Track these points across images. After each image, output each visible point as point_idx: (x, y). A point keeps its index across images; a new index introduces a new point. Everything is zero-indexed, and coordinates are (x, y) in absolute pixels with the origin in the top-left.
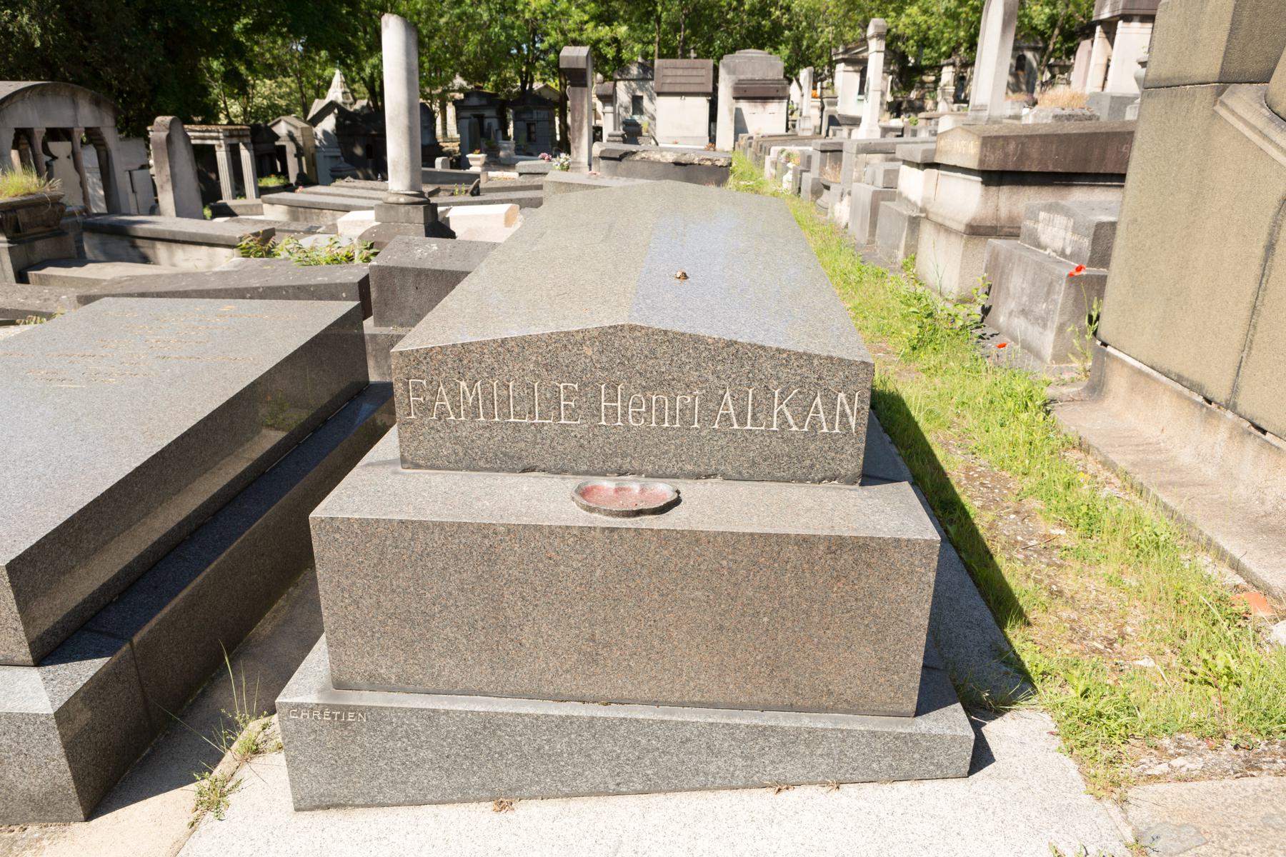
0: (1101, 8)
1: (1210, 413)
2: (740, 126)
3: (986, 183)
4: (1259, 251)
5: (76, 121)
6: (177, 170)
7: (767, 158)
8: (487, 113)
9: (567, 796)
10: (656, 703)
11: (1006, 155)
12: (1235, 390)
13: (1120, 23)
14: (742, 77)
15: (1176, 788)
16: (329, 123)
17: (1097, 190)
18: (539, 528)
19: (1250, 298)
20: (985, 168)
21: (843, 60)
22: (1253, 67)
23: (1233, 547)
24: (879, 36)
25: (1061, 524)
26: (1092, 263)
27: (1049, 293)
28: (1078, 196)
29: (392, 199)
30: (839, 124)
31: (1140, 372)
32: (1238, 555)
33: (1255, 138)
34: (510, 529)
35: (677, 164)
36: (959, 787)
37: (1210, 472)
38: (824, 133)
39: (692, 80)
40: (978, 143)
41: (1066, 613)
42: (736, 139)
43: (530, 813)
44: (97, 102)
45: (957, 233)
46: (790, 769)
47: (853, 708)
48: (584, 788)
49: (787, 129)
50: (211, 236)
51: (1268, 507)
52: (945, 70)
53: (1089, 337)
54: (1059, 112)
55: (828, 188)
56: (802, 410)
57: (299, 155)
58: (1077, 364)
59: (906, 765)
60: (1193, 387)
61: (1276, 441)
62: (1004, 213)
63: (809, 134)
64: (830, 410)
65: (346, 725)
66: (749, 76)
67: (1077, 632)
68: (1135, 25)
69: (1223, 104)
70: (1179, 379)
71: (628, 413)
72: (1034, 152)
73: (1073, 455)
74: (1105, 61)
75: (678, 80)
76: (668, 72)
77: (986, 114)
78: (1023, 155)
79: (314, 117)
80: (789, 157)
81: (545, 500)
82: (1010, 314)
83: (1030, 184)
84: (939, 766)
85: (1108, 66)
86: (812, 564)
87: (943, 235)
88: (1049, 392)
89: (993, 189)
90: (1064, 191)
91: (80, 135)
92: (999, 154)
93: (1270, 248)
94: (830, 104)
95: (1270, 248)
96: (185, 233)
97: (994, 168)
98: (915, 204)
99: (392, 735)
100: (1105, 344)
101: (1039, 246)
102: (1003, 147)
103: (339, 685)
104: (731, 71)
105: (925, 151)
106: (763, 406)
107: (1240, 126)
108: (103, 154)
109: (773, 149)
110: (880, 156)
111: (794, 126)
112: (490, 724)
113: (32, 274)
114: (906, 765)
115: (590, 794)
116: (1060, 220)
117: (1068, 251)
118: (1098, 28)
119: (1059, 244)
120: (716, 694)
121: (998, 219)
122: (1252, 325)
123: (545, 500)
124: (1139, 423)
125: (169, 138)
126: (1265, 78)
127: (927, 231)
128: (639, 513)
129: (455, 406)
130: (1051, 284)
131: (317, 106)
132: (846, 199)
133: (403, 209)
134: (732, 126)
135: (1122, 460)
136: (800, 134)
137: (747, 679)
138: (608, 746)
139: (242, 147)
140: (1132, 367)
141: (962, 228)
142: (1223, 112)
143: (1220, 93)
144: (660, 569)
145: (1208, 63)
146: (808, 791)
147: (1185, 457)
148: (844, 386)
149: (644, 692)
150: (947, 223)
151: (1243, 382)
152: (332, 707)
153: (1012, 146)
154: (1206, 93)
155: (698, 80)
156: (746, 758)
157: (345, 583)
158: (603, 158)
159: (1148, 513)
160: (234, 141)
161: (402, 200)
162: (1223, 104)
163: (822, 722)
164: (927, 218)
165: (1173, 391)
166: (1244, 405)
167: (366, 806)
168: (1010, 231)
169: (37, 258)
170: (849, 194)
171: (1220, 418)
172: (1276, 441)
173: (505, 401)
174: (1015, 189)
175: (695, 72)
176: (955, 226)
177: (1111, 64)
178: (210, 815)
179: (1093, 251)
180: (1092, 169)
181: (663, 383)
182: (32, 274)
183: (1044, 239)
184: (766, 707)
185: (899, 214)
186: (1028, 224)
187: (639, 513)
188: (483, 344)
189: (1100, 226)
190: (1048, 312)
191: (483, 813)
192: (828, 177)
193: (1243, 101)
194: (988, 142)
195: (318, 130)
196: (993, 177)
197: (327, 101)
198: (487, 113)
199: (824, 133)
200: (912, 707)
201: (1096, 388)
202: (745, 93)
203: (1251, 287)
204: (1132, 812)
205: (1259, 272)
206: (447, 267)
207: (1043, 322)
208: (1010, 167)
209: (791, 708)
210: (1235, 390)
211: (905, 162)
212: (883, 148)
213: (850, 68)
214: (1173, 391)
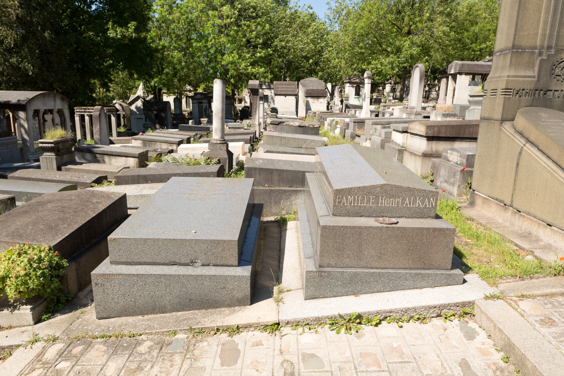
0: (451, 69)
1: (506, 208)
2: (308, 108)
4: (515, 165)
5: (55, 106)
6: (101, 127)
7: (325, 122)
8: (204, 101)
9: (372, 293)
10: (394, 268)
11: (434, 131)
12: (512, 201)
13: (458, 75)
14: (308, 88)
15: (507, 284)
16: (139, 103)
18: (372, 227)
19: (514, 177)
21: (349, 82)
22: (509, 117)
23: (516, 241)
24: (369, 78)
25: (469, 239)
26: (467, 166)
27: (454, 176)
28: (458, 145)
29: (215, 142)
30: (349, 108)
31: (485, 198)
32: (516, 242)
33: (511, 136)
34: (365, 227)
35: (299, 126)
36: (461, 286)
37: (507, 224)
39: (289, 89)
40: (425, 127)
41: (476, 257)
42: (307, 113)
44: (62, 99)
45: (419, 156)
46: (424, 283)
47: (437, 269)
48: (376, 290)
49: (328, 109)
50: (127, 153)
51: (523, 231)
52: (387, 85)
53: (468, 189)
54: (444, 112)
55: (359, 136)
56: (423, 202)
57: (124, 117)
58: (465, 197)
59: (449, 281)
60: (501, 201)
61: (523, 214)
62: (434, 149)
63: (338, 112)
64: (429, 202)
65: (322, 276)
66: (312, 88)
67: (479, 261)
68: (463, 76)
70: (497, 200)
71: (384, 202)
72: (443, 130)
73: (469, 222)
74: (453, 88)
75: (284, 89)
76: (279, 86)
78: (439, 132)
79: (131, 102)
80: (337, 123)
81: (371, 222)
82: (441, 182)
83: (442, 141)
84: (456, 281)
85: (454, 90)
86: (429, 234)
87: (413, 157)
88: (459, 205)
89: (430, 142)
90: (453, 143)
91: (55, 110)
92: (432, 131)
93: (518, 164)
94: (346, 100)
95: (518, 164)
96: (116, 152)
98: (399, 145)
99: (332, 278)
100: (474, 191)
101: (449, 161)
103: (320, 266)
104: (304, 86)
106: (415, 201)
107: (508, 133)
108: (63, 119)
109: (328, 119)
110: (380, 126)
111: (331, 108)
112: (356, 274)
113: (63, 168)
114: (449, 281)
115: (377, 292)
116: (455, 153)
117: (459, 163)
118: (450, 77)
119: (456, 161)
120: (407, 266)
121: (432, 151)
122: (515, 184)
123: (371, 222)
124: (486, 212)
125: (100, 114)
126: (513, 120)
127: (406, 156)
128: (392, 224)
129: (347, 202)
130: (455, 173)
131: (132, 97)
132: (368, 141)
133: (218, 145)
134: (305, 107)
135: (483, 222)
136: (335, 112)
137: (414, 262)
138: (382, 279)
139: (112, 116)
140: (483, 197)
141: (421, 154)
142: (503, 129)
143: (502, 123)
144: (397, 236)
145: (498, 115)
146: (427, 289)
147: (500, 221)
148: (432, 197)
149: (391, 266)
150: (414, 152)
151: (514, 199)
152: (319, 272)
153: (436, 129)
154: (497, 123)
155: (292, 90)
156: (413, 281)
157: (326, 241)
158: (272, 124)
159: (493, 234)
160: (110, 113)
161: (218, 142)
163: (430, 272)
164: (406, 150)
165: (495, 203)
166: (515, 205)
167: (323, 298)
168: (438, 155)
169: (64, 161)
170: (370, 139)
171: (509, 209)
172: (523, 214)
173: (358, 201)
174: (437, 142)
175: (290, 87)
176: (417, 153)
177: (456, 90)
178: (280, 303)
179: (467, 163)
180: (461, 136)
181: (393, 196)
182: (63, 168)
183: (450, 159)
184: (418, 269)
185: (394, 148)
186: (444, 154)
187: (392, 224)
188: (355, 188)
189: (468, 156)
190: (454, 181)
191: (353, 297)
192: (358, 132)
193: (507, 126)
194: (428, 127)
195: (133, 107)
196: (430, 138)
197: (136, 96)
198: (204, 101)
200: (450, 268)
201: (472, 203)
202: (311, 94)
203: (514, 174)
204: (499, 288)
206: (269, 167)
207: (453, 184)
208: (436, 135)
209: (424, 269)
210: (512, 201)
211: (394, 130)
214: (495, 203)
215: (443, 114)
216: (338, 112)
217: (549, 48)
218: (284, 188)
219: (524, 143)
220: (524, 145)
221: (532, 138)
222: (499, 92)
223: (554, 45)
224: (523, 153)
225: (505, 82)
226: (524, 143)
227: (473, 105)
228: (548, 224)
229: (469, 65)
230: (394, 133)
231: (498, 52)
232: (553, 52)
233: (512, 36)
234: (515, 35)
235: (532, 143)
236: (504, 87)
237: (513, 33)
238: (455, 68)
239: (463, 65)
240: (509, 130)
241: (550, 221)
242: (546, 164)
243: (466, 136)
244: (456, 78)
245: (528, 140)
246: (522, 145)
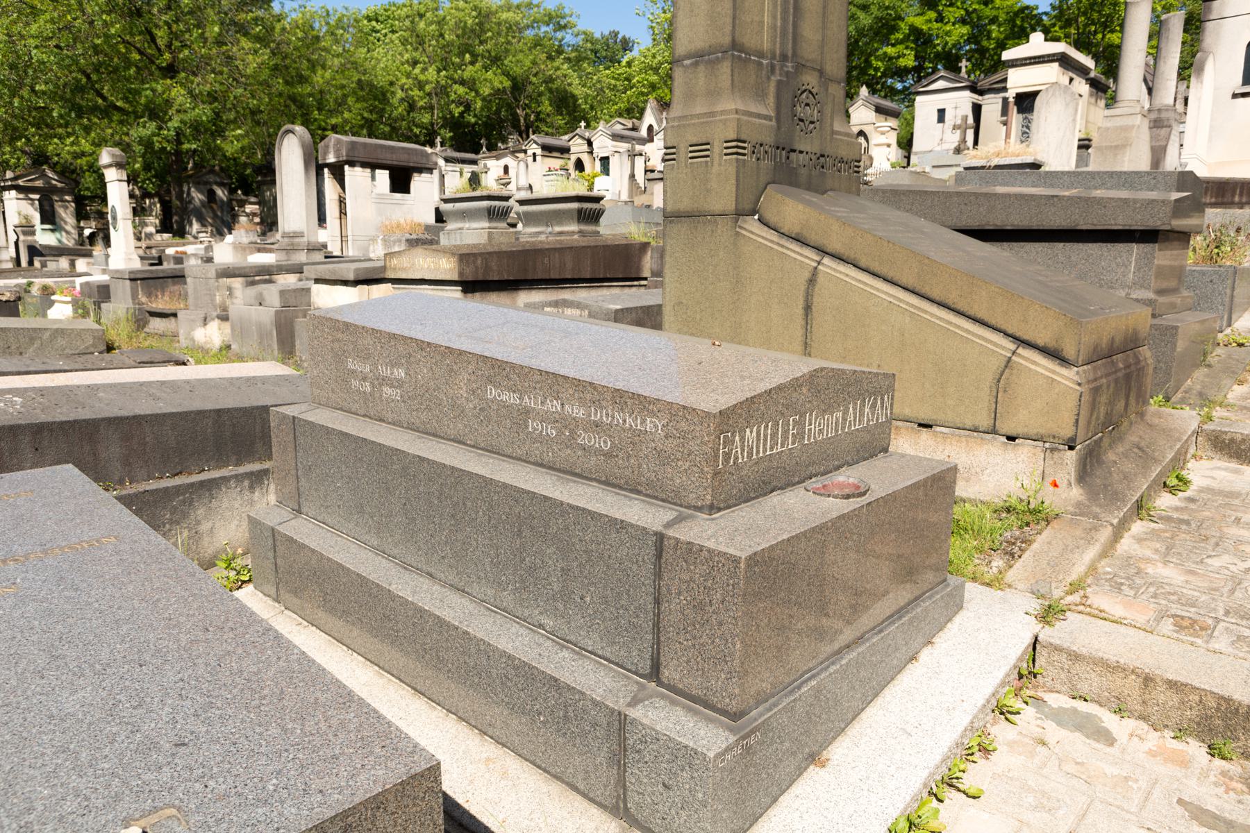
0: (326, 153)
3: (465, 291)
4: (799, 310)
11: (477, 268)
13: (346, 167)
17: (534, 292)
20: (464, 279)
22: (748, 206)
33: (776, 247)
38: (24, 263)
43: (839, 751)
54: (408, 236)
68: (358, 169)
69: (741, 227)
71: (820, 428)
72: (493, 264)
77: (305, 239)
78: (487, 268)
83: (493, 290)
90: (514, 294)
93: (808, 308)
95: (808, 308)
97: (470, 279)
102: (474, 262)
105: (356, 270)
118: (326, 170)
153: (479, 261)
162: (741, 227)
174: (484, 294)
180: (530, 277)
191: (812, 772)
199: (24, 263)
203: (799, 333)
205: (803, 323)
208: (481, 278)
211: (317, 281)
212: (242, 272)
213: (21, 196)
215: (407, 240)
216: (10, 265)
217: (784, 58)
218: (153, 485)
219: (818, 258)
220: (819, 263)
221: (835, 245)
222: (717, 148)
223: (790, 54)
224: (821, 279)
225: (733, 125)
226: (818, 258)
227: (456, 221)
228: (920, 425)
229: (365, 145)
230: (316, 288)
231: (687, 57)
232: (790, 66)
233: (729, 20)
234: (734, 18)
235: (835, 256)
236: (733, 136)
237: (730, 12)
238: (337, 153)
239: (353, 143)
240: (764, 234)
241: (925, 417)
242: (891, 295)
243: (540, 275)
244: (344, 175)
245: (823, 252)
246: (815, 264)
